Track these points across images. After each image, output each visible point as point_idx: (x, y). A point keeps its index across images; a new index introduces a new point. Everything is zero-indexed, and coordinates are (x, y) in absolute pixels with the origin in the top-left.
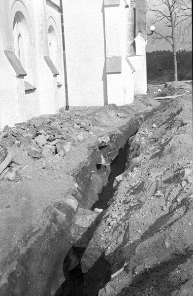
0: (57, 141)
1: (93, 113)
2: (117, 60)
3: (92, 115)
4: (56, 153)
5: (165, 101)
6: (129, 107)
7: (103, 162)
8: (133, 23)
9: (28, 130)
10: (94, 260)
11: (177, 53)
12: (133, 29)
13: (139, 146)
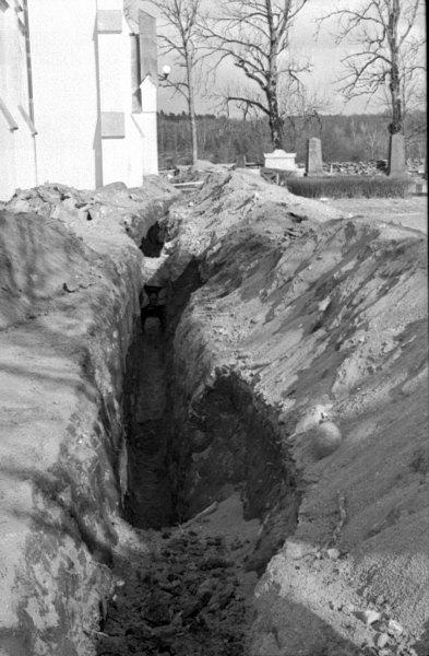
2: (118, 117)
5: (187, 189)
10: (184, 267)
12: (135, 69)
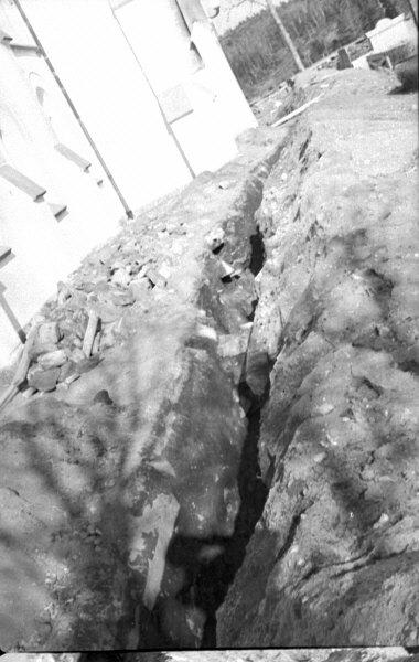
0: (145, 269)
1: (178, 203)
3: (179, 208)
4: (153, 285)
6: (235, 164)
7: (229, 270)
8: (176, 10)
9: (94, 272)
11: (277, 10)
13: (271, 219)
